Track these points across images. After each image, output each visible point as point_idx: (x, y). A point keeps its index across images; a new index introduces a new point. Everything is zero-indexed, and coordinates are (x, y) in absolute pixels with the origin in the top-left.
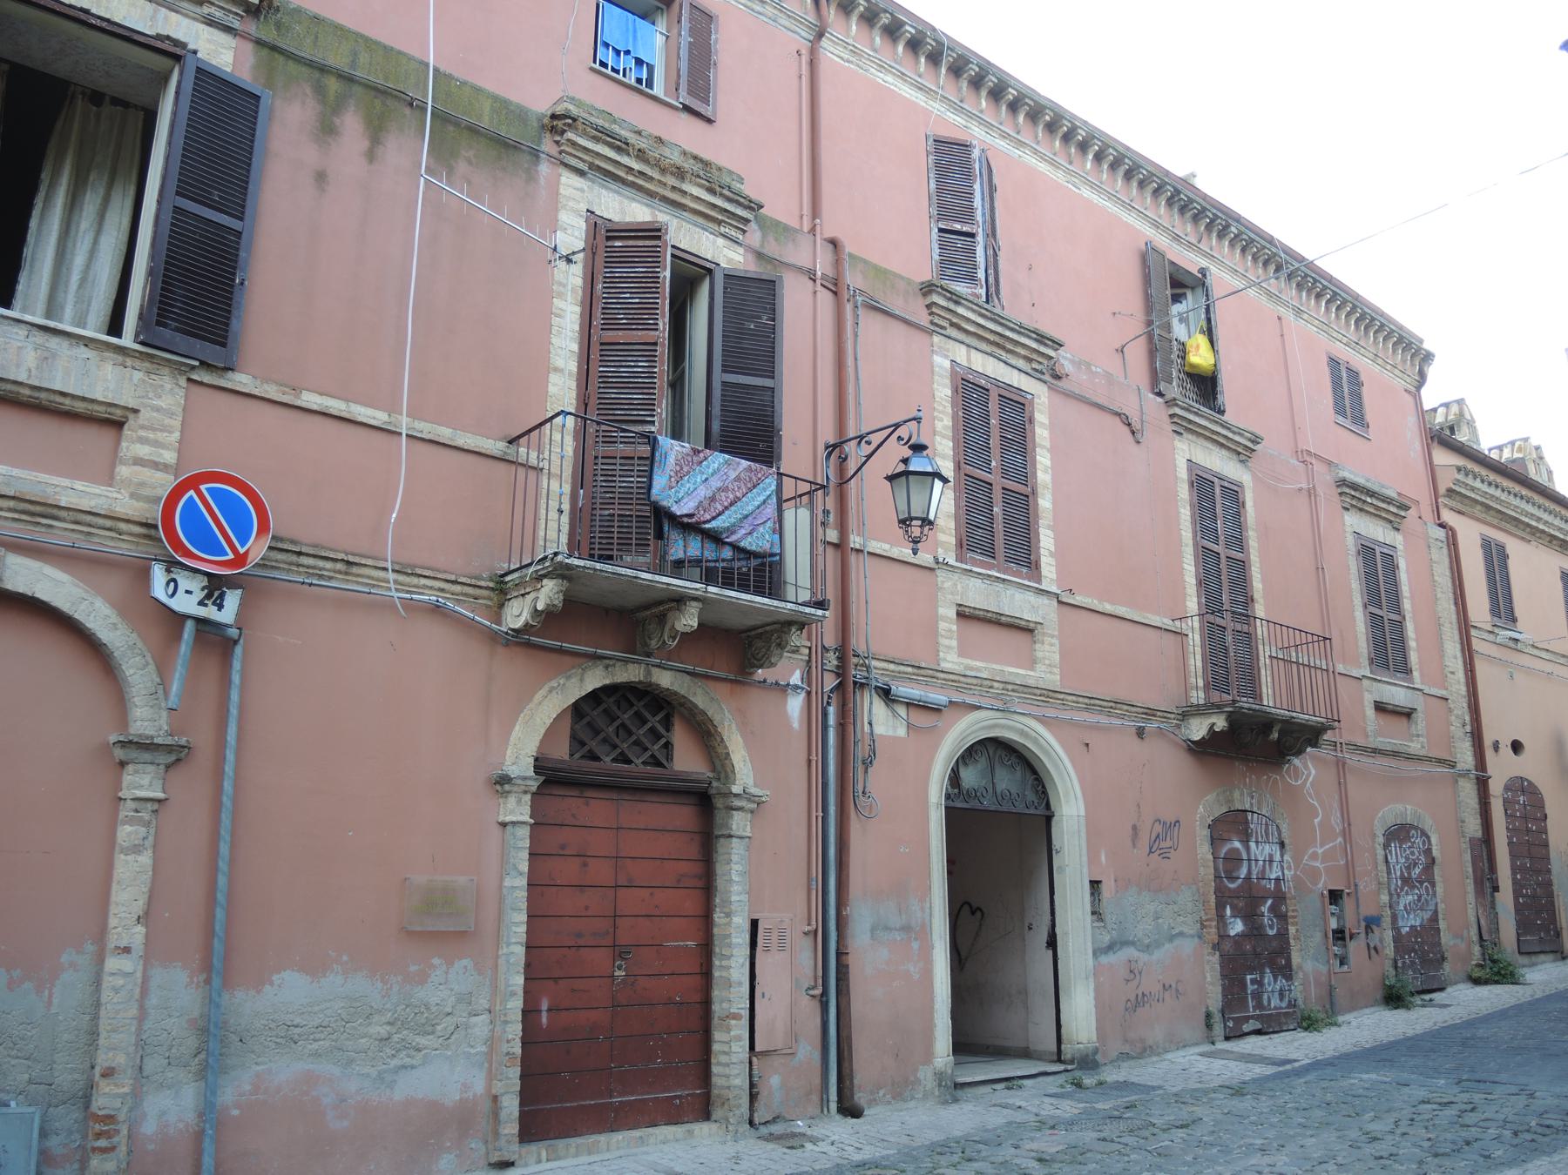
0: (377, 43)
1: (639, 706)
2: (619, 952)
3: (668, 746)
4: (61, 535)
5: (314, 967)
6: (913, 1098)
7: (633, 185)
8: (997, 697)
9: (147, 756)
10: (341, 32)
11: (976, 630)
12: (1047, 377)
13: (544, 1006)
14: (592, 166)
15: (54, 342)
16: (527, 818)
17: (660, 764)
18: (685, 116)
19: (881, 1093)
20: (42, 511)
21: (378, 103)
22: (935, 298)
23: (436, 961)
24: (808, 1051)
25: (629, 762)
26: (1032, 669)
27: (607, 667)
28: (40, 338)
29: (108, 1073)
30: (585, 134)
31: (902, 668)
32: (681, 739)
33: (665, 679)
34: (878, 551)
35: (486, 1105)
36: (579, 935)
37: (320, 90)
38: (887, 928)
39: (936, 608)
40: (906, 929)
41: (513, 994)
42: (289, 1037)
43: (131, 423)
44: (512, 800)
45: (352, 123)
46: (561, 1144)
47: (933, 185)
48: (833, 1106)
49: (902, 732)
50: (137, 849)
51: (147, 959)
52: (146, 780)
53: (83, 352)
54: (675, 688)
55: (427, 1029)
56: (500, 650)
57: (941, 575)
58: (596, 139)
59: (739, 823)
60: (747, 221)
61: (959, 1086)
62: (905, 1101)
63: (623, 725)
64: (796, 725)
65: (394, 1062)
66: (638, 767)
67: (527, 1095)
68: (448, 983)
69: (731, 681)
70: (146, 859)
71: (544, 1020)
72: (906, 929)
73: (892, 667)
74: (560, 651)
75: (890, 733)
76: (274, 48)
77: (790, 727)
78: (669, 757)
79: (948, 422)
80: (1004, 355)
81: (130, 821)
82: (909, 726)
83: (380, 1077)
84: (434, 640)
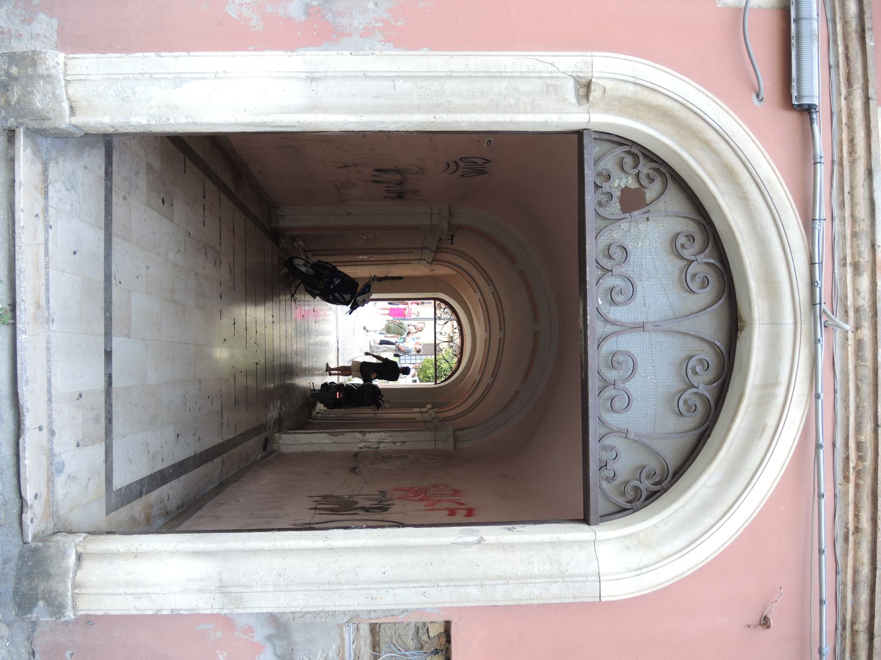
8: (839, 298)
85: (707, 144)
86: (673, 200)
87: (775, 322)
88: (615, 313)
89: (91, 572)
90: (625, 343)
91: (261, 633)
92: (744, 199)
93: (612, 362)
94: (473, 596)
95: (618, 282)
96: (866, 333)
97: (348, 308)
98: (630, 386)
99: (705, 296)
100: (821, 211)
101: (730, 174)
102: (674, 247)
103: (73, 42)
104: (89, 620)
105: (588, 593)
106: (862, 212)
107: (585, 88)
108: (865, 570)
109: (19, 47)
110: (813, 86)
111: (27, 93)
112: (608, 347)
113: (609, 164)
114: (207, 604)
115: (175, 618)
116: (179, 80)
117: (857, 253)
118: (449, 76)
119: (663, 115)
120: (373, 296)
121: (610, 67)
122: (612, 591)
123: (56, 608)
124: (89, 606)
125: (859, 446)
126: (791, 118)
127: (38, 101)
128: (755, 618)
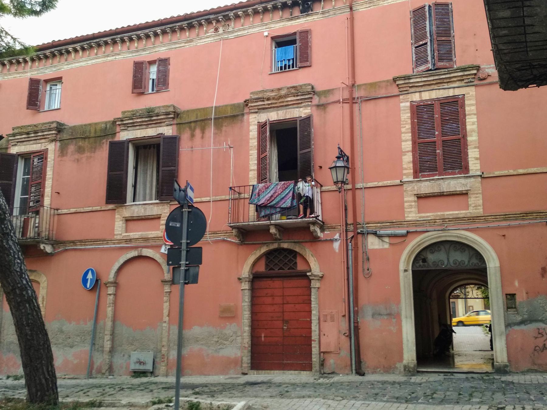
0: (201, 109)
1: (286, 253)
2: (285, 321)
3: (296, 263)
4: (151, 243)
5: (201, 325)
6: (393, 373)
7: (271, 108)
8: (440, 225)
9: (166, 283)
10: (193, 111)
11: (422, 201)
12: (476, 82)
13: (263, 336)
14: (258, 109)
15: (146, 206)
16: (247, 288)
17: (293, 269)
18: (301, 70)
19: (378, 370)
20: (147, 239)
21: (203, 123)
22: (398, 83)
23: (227, 324)
24: (345, 353)
25: (284, 269)
26: (468, 209)
27: (267, 246)
28: (144, 206)
29: (163, 346)
30: (253, 102)
31: (384, 224)
32: (299, 260)
33: (285, 246)
34: (372, 186)
35: (240, 359)
36: (272, 317)
37: (190, 128)
38: (380, 314)
39: (403, 198)
40: (389, 314)
41: (245, 332)
42: (197, 340)
43: (162, 216)
44: (243, 284)
45: (198, 132)
46: (260, 371)
47: (413, 31)
48: (354, 371)
49: (387, 246)
50: (166, 302)
51: (169, 323)
52: (167, 288)
53: (151, 206)
54: (289, 247)
55: (227, 340)
56: (241, 247)
57: (405, 186)
58: (257, 102)
59: (315, 284)
60: (311, 98)
61: (418, 372)
62: (390, 373)
63: (281, 259)
64: (337, 251)
65: (219, 347)
66: (286, 271)
67: (252, 358)
68: (230, 329)
69: (311, 242)
70: (168, 304)
71: (263, 339)
72: (389, 314)
73: (379, 225)
74: (253, 244)
75: (381, 247)
76: (180, 124)
77: (335, 252)
78: (296, 267)
79: (409, 126)
80: (446, 86)
81: (165, 297)
82: (390, 244)
83: (216, 350)
84: (223, 247)
85: (414, 249)
86: (424, 253)
87: (446, 236)
88: (446, 263)
89: (499, 360)
90: (451, 261)
91: (510, 329)
92: (424, 242)
93: (455, 264)
94: (500, 290)
95: (440, 263)
96: (447, 220)
97: (454, 334)
98: (460, 261)
99: (442, 247)
100: (424, 229)
101: (419, 245)
102: (433, 253)
103: (401, 359)
104: (509, 361)
105: (498, 269)
106: (425, 222)
107: (406, 271)
108: (493, 217)
109: (402, 370)
110: (404, 231)
111: (411, 368)
112: (452, 265)
113: (418, 265)
114: (504, 338)
115: (507, 344)
116: (408, 341)
117: (432, 222)
118: (405, 294)
119: (409, 257)
120: (449, 323)
121: (402, 267)
122: (498, 264)
123: (506, 366)
124: (506, 360)
125: (468, 220)
126: (409, 235)
127: (412, 366)
128: (503, 237)
